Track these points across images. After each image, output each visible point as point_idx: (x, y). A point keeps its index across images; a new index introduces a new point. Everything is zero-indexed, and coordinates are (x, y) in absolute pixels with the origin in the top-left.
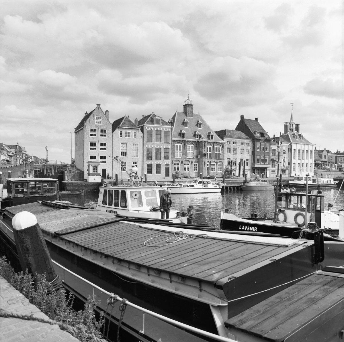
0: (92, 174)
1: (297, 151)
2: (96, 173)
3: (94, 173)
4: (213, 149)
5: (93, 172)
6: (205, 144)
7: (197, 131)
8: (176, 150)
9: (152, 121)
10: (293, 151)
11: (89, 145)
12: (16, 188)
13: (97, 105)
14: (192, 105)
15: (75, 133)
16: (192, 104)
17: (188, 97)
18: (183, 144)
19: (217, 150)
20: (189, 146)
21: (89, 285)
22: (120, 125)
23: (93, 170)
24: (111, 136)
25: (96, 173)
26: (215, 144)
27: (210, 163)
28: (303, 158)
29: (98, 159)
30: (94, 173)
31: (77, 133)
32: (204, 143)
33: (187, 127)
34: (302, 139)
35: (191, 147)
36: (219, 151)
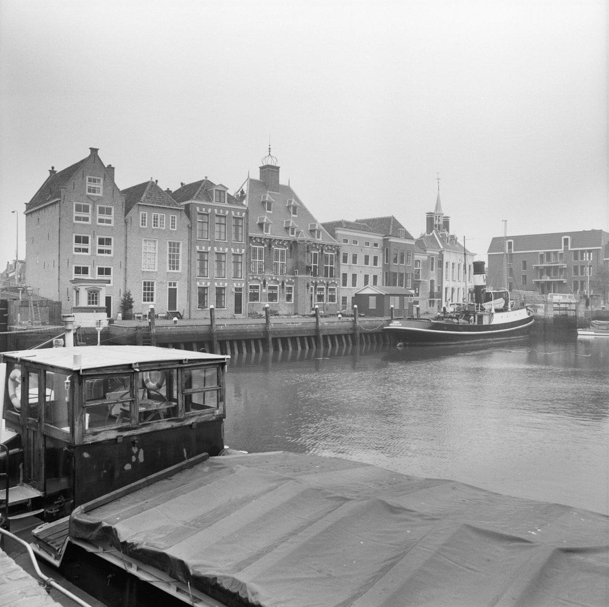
0: (88, 308)
1: (450, 266)
2: (95, 306)
3: (91, 306)
4: (320, 257)
5: (89, 304)
9: (208, 196)
11: (72, 241)
13: (91, 149)
15: (27, 215)
16: (277, 165)
21: (61, 594)
22: (142, 199)
23: (89, 298)
24: (123, 224)
25: (95, 306)
27: (316, 284)
28: (469, 280)
29: (93, 275)
30: (91, 306)
31: (35, 215)
36: (332, 263)
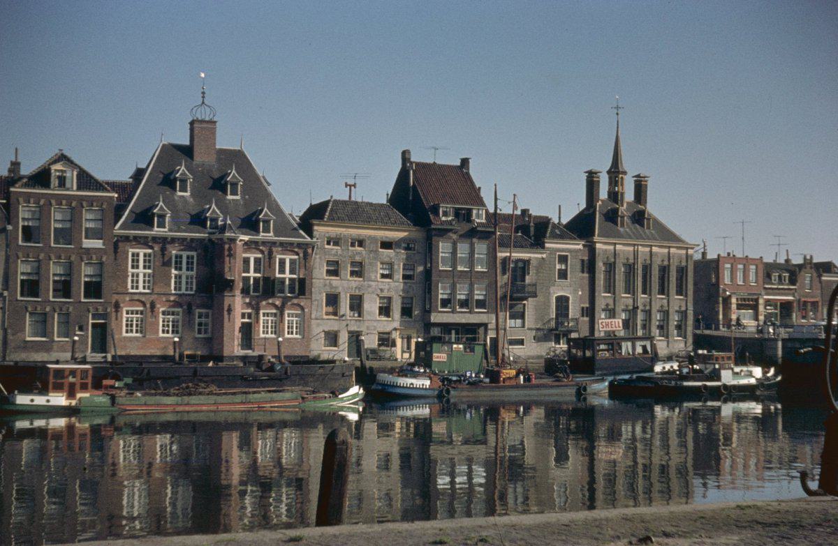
4: (267, 264)
6: (230, 249)
7: (265, 209)
8: (133, 267)
10: (600, 266)
12: (244, 275)
14: (215, 122)
16: (215, 120)
17: (203, 97)
18: (157, 248)
19: (284, 268)
20: (138, 255)
26: (274, 249)
32: (227, 246)
33: (238, 197)
34: (649, 228)
35: (188, 257)
